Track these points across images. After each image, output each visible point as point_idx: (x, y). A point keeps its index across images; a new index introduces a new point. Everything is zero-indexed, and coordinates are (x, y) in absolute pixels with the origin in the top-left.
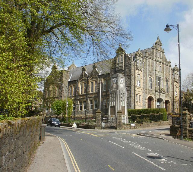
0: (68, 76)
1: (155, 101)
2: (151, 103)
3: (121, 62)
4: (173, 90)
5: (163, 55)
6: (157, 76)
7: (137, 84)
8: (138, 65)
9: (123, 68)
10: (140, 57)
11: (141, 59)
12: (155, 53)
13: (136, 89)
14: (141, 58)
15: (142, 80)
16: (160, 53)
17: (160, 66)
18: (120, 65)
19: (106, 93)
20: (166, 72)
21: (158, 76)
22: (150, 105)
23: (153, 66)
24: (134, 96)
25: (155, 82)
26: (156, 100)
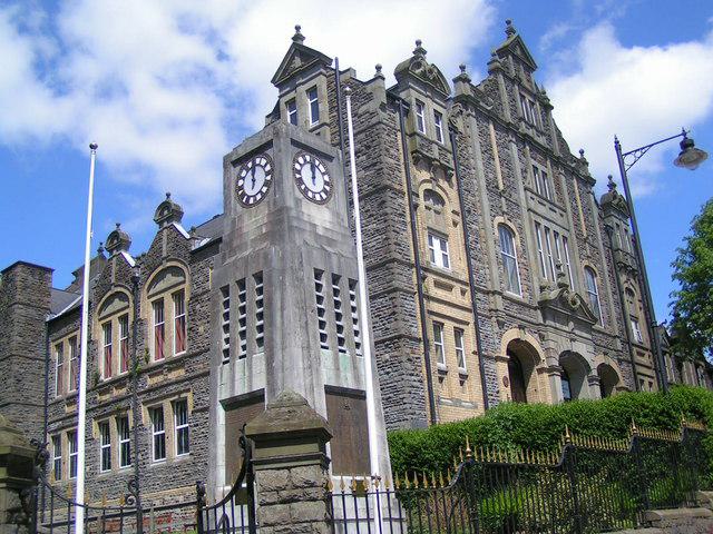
20: (575, 209)
23: (506, 162)
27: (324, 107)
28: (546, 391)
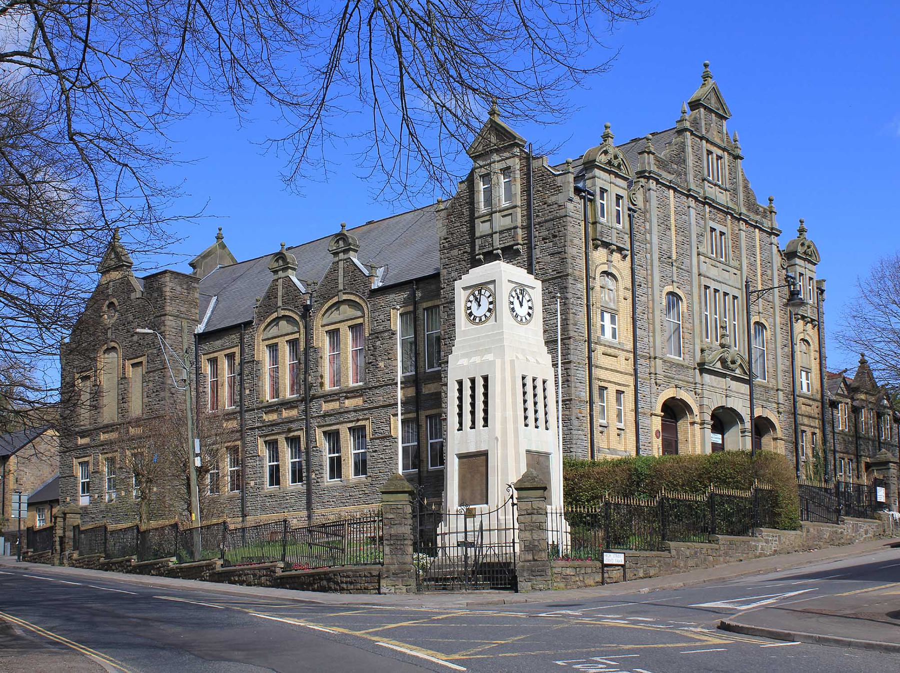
0: (193, 303)
1: (702, 423)
2: (680, 436)
3: (504, 204)
4: (788, 363)
5: (733, 171)
6: (707, 287)
7: (603, 327)
8: (602, 220)
9: (514, 237)
10: (617, 175)
11: (617, 187)
12: (691, 160)
13: (599, 358)
14: (619, 181)
15: (625, 308)
16: (719, 158)
17: (719, 228)
18: (501, 222)
19: (418, 392)
20: (752, 265)
21: (713, 285)
22: (670, 444)
23: (683, 230)
24: (585, 396)
25: (697, 322)
26: (708, 418)
27: (517, 188)
28: (697, 441)
